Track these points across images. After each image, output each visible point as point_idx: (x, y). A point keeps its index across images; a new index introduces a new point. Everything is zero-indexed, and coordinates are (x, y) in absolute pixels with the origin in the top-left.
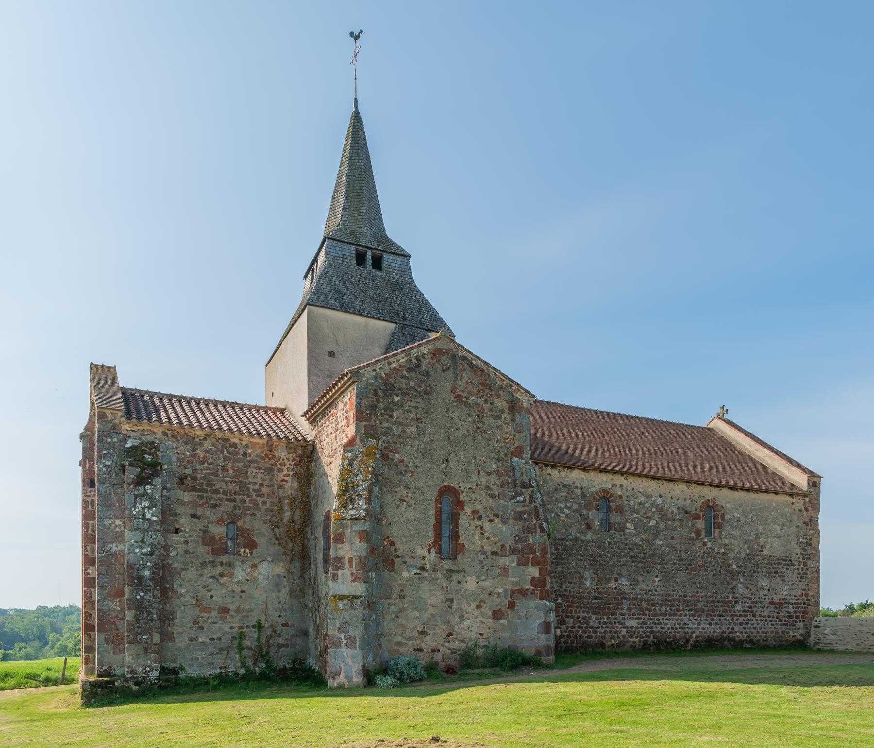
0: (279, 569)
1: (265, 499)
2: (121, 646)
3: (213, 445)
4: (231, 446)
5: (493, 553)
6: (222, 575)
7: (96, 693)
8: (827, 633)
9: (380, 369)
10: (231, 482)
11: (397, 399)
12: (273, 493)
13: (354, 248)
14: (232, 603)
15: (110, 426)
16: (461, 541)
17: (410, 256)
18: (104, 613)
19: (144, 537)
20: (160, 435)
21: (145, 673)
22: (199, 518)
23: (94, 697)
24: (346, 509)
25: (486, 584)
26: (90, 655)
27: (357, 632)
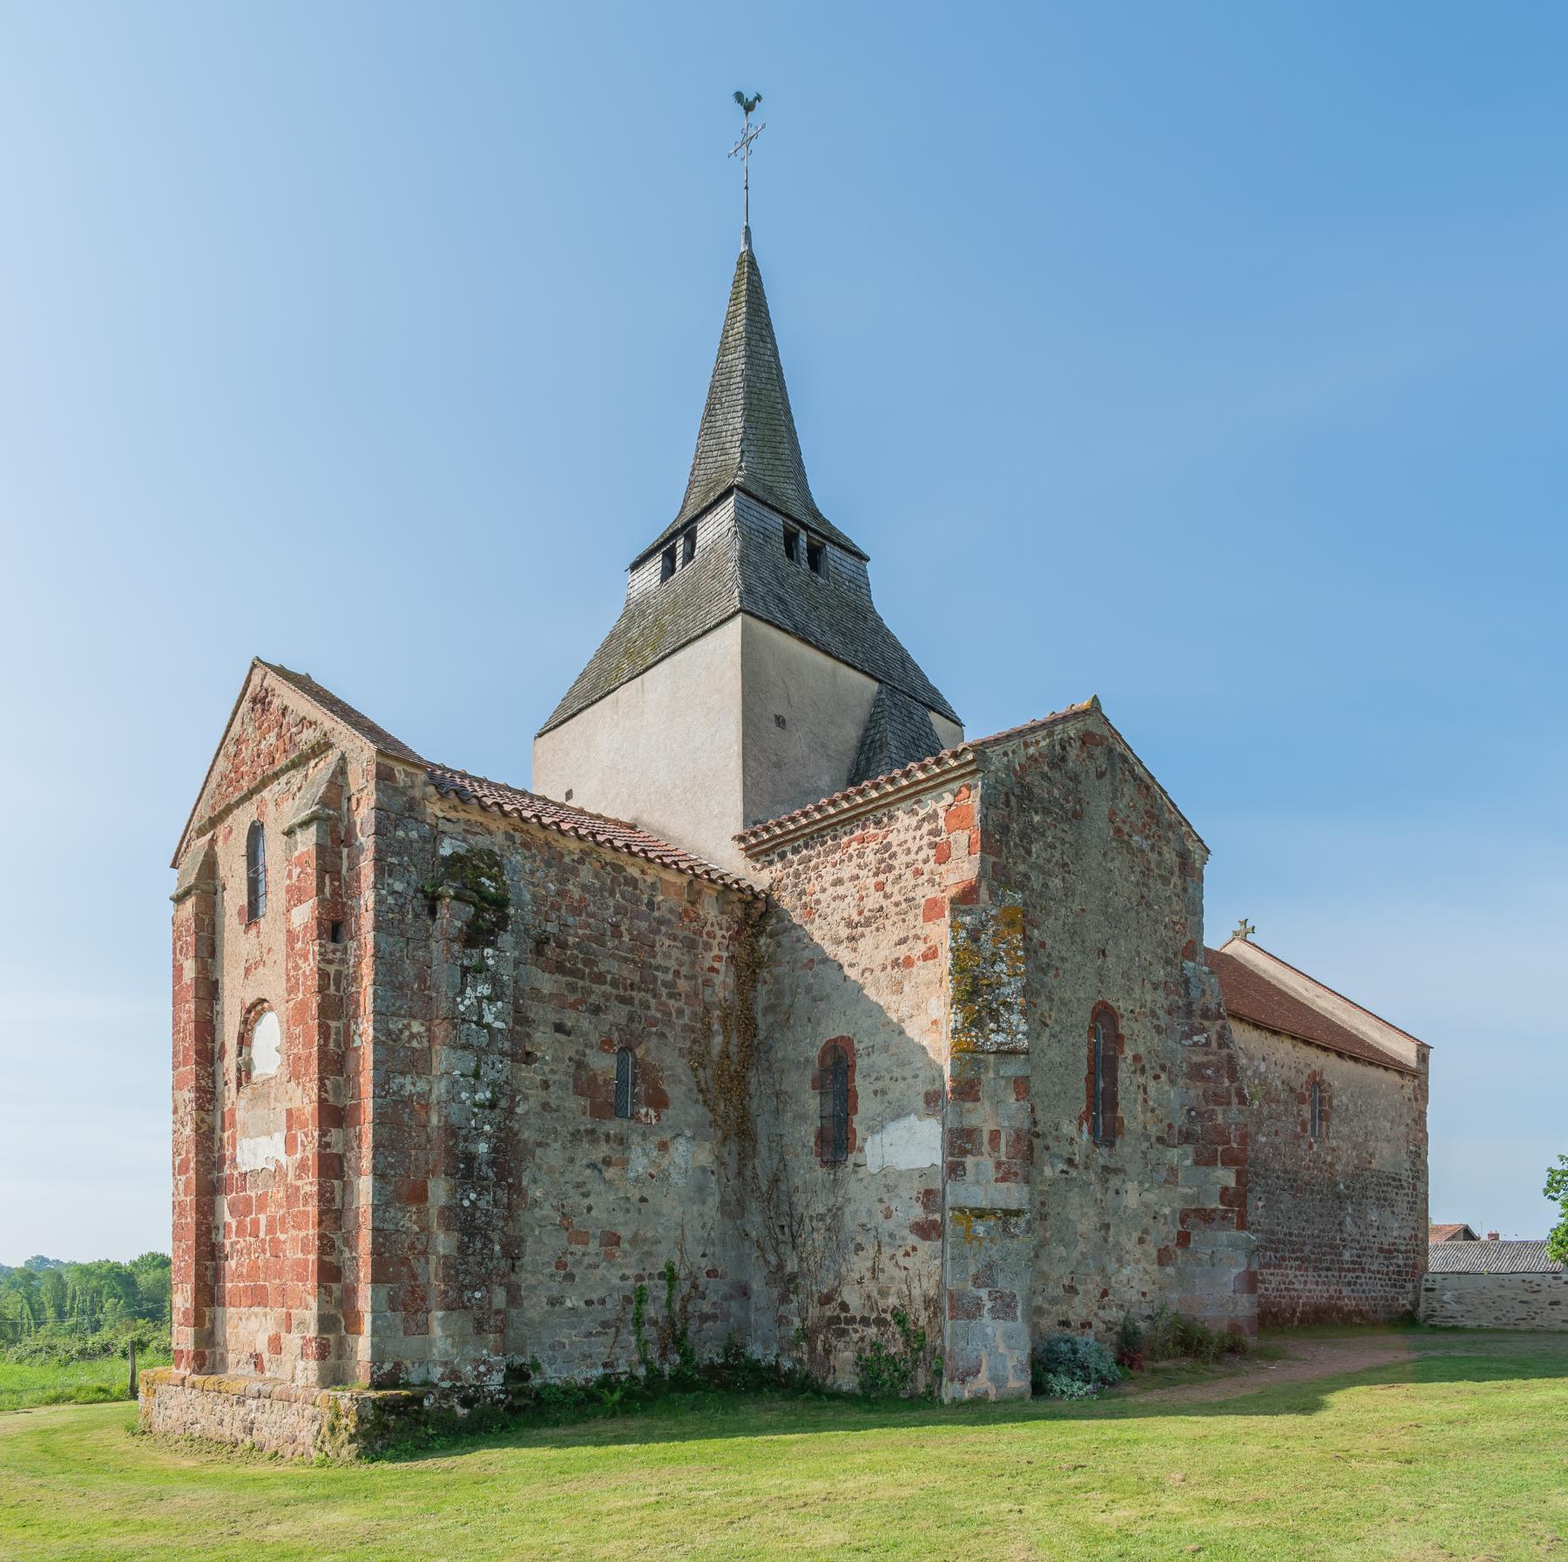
0: (704, 1157)
1: (681, 1004)
2: (420, 1316)
3: (597, 876)
4: (627, 883)
5: (1160, 1140)
6: (607, 1162)
7: (386, 1427)
8: (1448, 1303)
9: (1014, 752)
10: (626, 960)
11: (1037, 818)
12: (696, 994)
13: (779, 520)
14: (626, 1223)
15: (401, 800)
16: (1120, 1113)
17: (868, 560)
18: (386, 1238)
19: (478, 1066)
20: (500, 838)
21: (477, 1377)
22: (568, 1034)
23: (382, 1436)
24: (981, 1029)
25: (1150, 1197)
26: (331, 1337)
27: (1014, 1285)
